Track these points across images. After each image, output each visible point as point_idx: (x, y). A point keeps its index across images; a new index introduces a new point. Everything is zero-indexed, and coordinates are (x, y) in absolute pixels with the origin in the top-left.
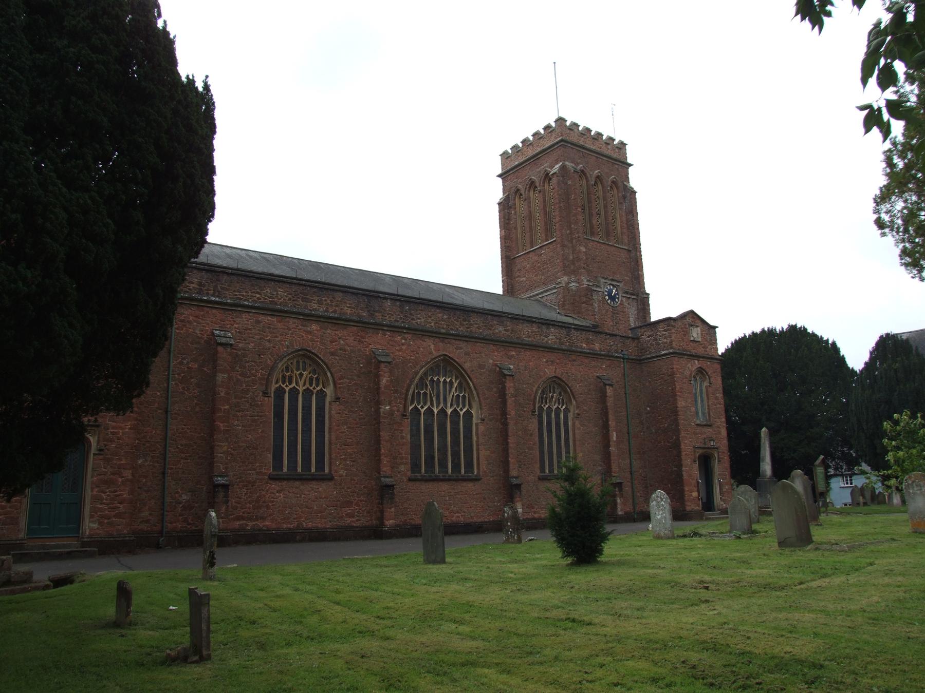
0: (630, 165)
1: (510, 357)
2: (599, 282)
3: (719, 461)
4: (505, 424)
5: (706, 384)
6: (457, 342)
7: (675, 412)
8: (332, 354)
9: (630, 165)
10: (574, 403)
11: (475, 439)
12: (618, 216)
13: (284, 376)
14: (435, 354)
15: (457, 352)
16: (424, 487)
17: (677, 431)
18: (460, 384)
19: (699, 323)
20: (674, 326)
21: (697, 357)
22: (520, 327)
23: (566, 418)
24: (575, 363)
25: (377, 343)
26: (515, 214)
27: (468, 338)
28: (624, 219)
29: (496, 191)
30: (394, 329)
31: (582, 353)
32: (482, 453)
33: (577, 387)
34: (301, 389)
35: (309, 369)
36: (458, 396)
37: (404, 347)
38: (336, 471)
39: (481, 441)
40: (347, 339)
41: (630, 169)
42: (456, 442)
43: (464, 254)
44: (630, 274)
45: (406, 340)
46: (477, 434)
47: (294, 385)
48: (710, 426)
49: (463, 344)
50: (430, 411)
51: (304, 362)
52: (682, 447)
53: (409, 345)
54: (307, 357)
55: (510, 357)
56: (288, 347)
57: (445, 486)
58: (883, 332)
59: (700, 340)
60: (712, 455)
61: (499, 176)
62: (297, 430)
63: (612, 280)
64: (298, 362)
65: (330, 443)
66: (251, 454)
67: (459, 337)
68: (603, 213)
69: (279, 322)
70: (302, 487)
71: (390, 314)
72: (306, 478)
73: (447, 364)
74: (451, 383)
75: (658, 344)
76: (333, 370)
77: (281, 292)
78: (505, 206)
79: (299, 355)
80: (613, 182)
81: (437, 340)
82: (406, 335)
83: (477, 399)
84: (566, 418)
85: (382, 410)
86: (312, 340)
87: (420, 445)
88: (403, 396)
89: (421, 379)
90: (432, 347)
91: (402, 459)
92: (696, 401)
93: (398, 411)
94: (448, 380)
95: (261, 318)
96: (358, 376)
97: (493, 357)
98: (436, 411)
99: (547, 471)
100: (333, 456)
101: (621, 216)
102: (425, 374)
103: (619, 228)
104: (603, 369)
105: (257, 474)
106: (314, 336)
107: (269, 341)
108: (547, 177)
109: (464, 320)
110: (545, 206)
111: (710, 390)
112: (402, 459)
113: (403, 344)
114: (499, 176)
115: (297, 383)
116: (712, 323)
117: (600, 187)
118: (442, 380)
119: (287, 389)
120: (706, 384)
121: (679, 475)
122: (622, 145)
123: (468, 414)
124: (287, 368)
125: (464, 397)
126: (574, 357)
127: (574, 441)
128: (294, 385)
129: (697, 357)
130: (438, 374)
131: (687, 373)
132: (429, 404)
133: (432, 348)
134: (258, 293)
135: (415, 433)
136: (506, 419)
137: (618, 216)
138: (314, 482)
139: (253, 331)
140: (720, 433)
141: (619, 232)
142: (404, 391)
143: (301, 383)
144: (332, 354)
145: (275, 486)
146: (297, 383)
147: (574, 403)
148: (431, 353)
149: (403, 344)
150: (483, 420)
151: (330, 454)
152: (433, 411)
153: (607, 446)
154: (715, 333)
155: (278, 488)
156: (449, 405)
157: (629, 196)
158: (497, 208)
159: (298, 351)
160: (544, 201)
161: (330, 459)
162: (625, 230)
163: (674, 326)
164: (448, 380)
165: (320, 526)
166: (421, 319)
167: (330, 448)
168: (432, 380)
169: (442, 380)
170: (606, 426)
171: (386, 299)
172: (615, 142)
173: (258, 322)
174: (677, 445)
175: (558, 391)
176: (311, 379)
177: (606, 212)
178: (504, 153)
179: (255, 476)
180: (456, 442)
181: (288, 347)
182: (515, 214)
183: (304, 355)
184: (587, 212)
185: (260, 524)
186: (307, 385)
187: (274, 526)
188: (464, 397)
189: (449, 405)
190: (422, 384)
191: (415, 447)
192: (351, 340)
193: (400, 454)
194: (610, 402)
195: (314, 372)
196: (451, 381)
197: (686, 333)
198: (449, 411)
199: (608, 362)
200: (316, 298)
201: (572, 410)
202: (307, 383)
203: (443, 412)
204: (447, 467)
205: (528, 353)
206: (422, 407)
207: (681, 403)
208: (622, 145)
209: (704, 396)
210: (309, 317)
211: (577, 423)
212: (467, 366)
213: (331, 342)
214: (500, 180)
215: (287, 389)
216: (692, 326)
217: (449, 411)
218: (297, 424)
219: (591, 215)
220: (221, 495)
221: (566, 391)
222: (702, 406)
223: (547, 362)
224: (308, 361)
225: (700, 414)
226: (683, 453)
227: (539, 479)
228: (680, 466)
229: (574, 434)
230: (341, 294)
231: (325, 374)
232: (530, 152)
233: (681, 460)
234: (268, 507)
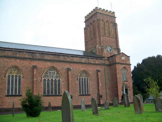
0: (116, 17)
1: (71, 66)
2: (106, 46)
3: (130, 90)
4: (68, 82)
5: (126, 71)
6: (56, 63)
7: (116, 78)
8: (22, 67)
9: (116, 17)
10: (89, 76)
11: (61, 86)
12: (112, 30)
13: (10, 72)
14: (50, 66)
15: (55, 65)
16: (46, 97)
17: (117, 83)
18: (57, 73)
19: (124, 55)
20: (117, 57)
21: (124, 64)
22: (74, 58)
23: (87, 80)
24: (90, 67)
25: (34, 63)
26: (88, 31)
27: (60, 61)
28: (114, 31)
29: (84, 25)
30: (39, 60)
31: (92, 64)
32: (62, 90)
33: (90, 73)
34: (14, 75)
35: (17, 70)
36: (56, 76)
37: (41, 65)
38: (23, 94)
39: (62, 86)
40: (26, 63)
41: (116, 19)
42: (56, 87)
43: (76, 43)
44: (115, 44)
45: (42, 63)
46: (61, 85)
47: (20, 75)
48: (127, 81)
49: (57, 63)
50: (48, 80)
51: (15, 69)
52: (118, 87)
53: (43, 64)
54: (16, 67)
55: (71, 66)
56: (11, 66)
57: (52, 98)
58: (149, 56)
59: (125, 60)
60: (128, 89)
61: (84, 22)
62: (13, 85)
63: (110, 46)
64: (14, 69)
65: (22, 88)
66: (1, 91)
67: (57, 61)
68: (108, 30)
69: (9, 60)
70: (14, 98)
71: (38, 56)
72: (16, 96)
73: (53, 68)
74: (55, 73)
75: (113, 61)
76: (23, 71)
77: (9, 53)
78: (85, 29)
79: (14, 67)
80: (107, 21)
81: (51, 62)
82: (42, 62)
83: (61, 76)
84: (87, 80)
85: (34, 80)
86: (17, 64)
87: (46, 88)
88: (41, 76)
89: (46, 72)
90: (49, 64)
91: (40, 91)
92: (123, 75)
93: (40, 80)
94: (54, 72)
95: (4, 59)
96: (29, 72)
97: (67, 66)
98: (50, 80)
99: (82, 94)
100: (22, 91)
101: (113, 30)
102: (48, 71)
103: (113, 33)
104: (98, 68)
105: (3, 95)
106: (18, 63)
107: (6, 64)
108: (94, 21)
109: (58, 57)
110: (94, 29)
111: (127, 72)
112: (40, 91)
113: (41, 64)
114: (84, 22)
115: (13, 74)
116: (128, 56)
117: (107, 23)
118: (52, 72)
119: (11, 75)
120: (126, 71)
121: (118, 94)
122: (114, 13)
123: (59, 80)
124: (11, 70)
125: (58, 76)
126: (90, 65)
127: (89, 86)
128: (13, 74)
129: (124, 64)
130: (51, 71)
131: (120, 68)
132: (59, 78)
133: (49, 64)
134: (4, 54)
135: (45, 85)
136: (69, 81)
137: (112, 30)
138: (17, 97)
139: (2, 62)
140: (130, 83)
141: (113, 34)
142: (41, 75)
143: (14, 74)
144: (22, 67)
145: (7, 98)
146: (13, 74)
147: (89, 76)
148: (49, 66)
149: (41, 64)
150: (63, 81)
151: (22, 90)
152: (49, 80)
153: (98, 87)
154: (129, 58)
155: (8, 99)
156: (54, 78)
157: (115, 25)
158: (84, 30)
159: (13, 66)
160: (94, 27)
161: (22, 91)
162: (114, 34)
163: (117, 57)
164: (54, 72)
165: (18, 107)
166: (46, 57)
167: (22, 89)
168: (49, 72)
169: (52, 72)
170: (98, 82)
171: (37, 53)
172: (112, 12)
173: (4, 60)
174: (117, 87)
175: (85, 74)
176: (17, 73)
177: (109, 29)
178: (85, 17)
179: (2, 96)
180: (56, 87)
181: (11, 66)
182: (88, 31)
183: (15, 67)
184: (104, 29)
185: (3, 107)
186: (16, 74)
187: (7, 107)
188: (58, 76)
189: (54, 78)
190: (46, 73)
191: (45, 88)
192: (27, 63)
193: (40, 90)
194: (99, 76)
195: (18, 71)
196: (54, 72)
197: (121, 58)
198: (54, 79)
199: (100, 66)
200: (19, 54)
201: (89, 79)
202: (16, 74)
203: (52, 80)
204: (53, 93)
205: (76, 65)
206: (57, 79)
207: (118, 76)
208: (114, 13)
209: (126, 74)
210: (16, 58)
211: (90, 82)
212: (59, 68)
213: (22, 64)
214: (85, 23)
215: (11, 75)
216: (122, 56)
217: (54, 79)
218: (13, 83)
219: (105, 30)
220: (101, 98)
221: (87, 74)
222: (125, 76)
223: (82, 67)
224: (16, 69)
225: (124, 78)
226: (119, 89)
227: (79, 96)
228: (118, 92)
229: (89, 84)
230: (25, 53)
231: (20, 71)
232: (90, 16)
233: (118, 90)
234: (5, 103)
